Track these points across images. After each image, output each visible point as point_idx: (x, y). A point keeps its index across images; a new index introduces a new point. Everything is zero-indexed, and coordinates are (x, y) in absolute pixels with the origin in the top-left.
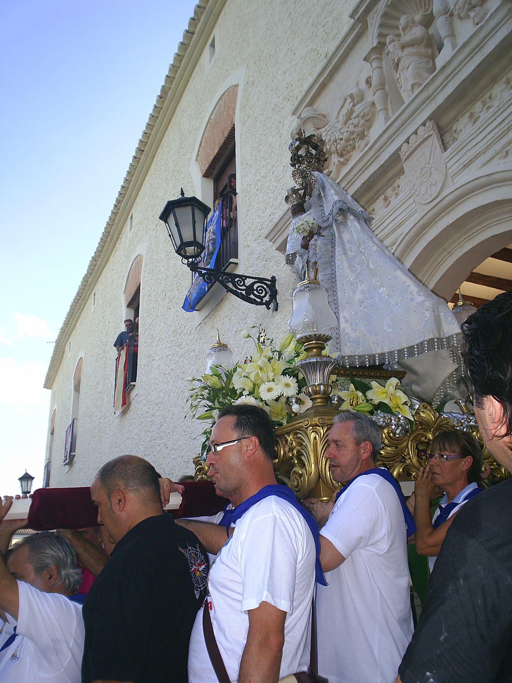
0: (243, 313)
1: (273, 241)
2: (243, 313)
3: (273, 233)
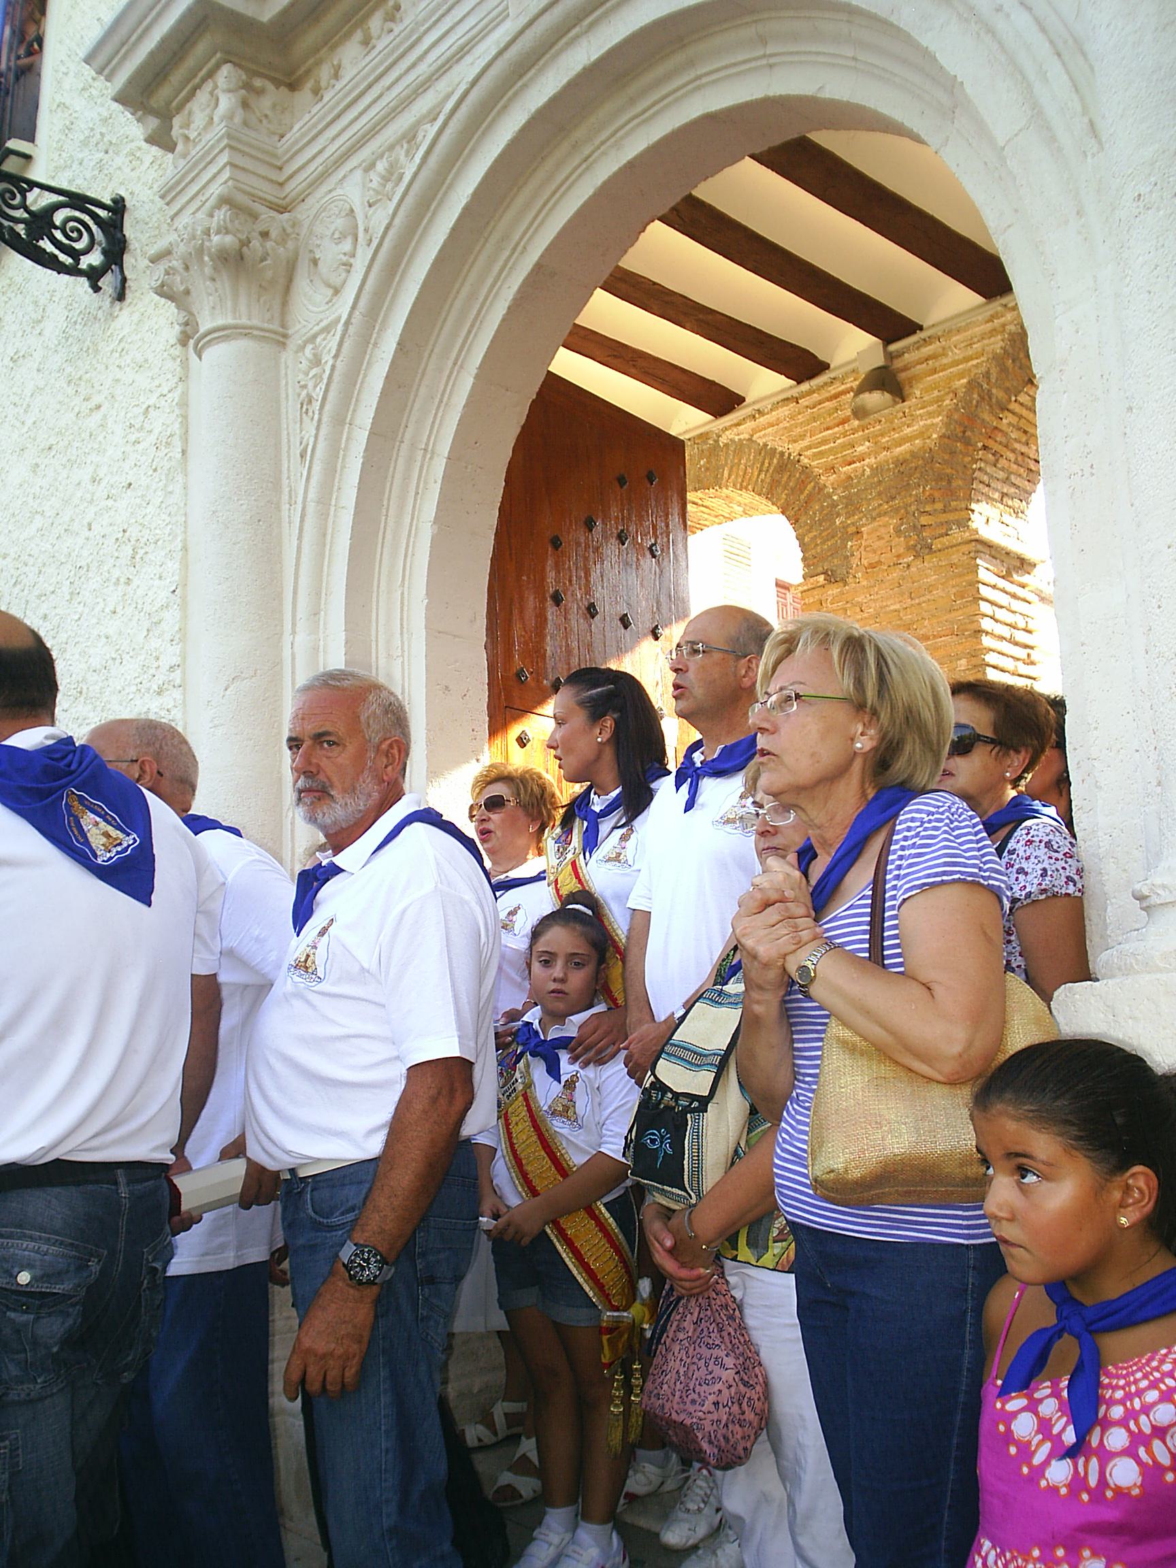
0: (36, 303)
1: (106, 72)
2: (36, 303)
3: (108, 50)
